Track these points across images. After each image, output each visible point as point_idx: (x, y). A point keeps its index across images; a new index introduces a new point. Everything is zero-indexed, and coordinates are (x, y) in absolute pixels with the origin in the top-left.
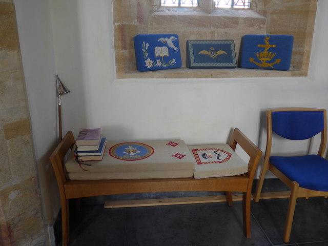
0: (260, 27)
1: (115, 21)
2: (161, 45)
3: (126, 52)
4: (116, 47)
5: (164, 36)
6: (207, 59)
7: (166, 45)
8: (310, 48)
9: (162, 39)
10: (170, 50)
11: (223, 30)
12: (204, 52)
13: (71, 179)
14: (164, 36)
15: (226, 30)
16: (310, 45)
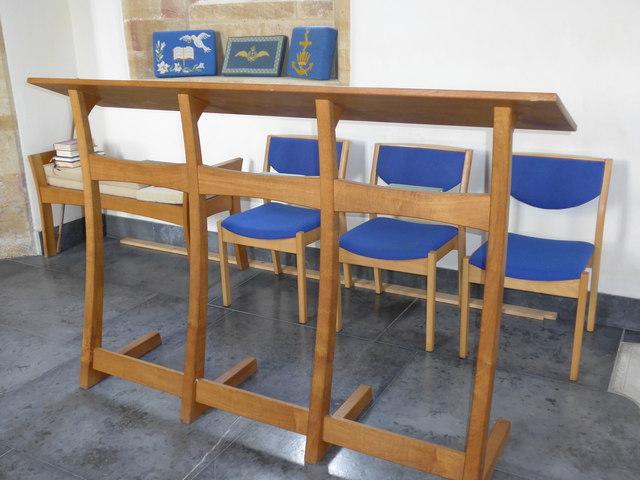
0: (325, 15)
1: (125, 17)
2: (184, 44)
3: (141, 54)
4: (128, 48)
5: (190, 33)
6: (244, 63)
7: (192, 44)
8: (348, 45)
9: (187, 38)
10: (198, 51)
11: (275, 22)
12: (243, 54)
13: (51, 183)
14: (190, 33)
15: (279, 21)
16: (348, 41)
